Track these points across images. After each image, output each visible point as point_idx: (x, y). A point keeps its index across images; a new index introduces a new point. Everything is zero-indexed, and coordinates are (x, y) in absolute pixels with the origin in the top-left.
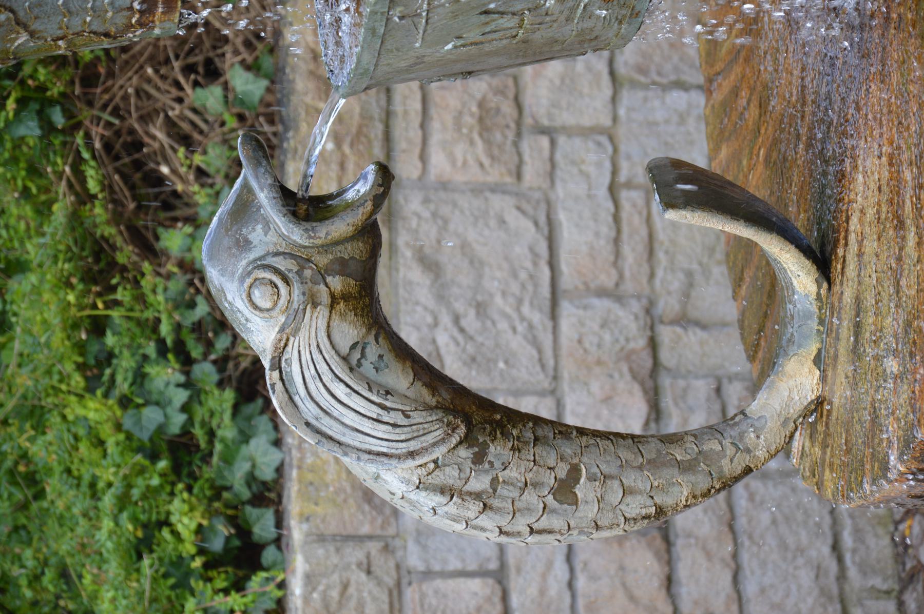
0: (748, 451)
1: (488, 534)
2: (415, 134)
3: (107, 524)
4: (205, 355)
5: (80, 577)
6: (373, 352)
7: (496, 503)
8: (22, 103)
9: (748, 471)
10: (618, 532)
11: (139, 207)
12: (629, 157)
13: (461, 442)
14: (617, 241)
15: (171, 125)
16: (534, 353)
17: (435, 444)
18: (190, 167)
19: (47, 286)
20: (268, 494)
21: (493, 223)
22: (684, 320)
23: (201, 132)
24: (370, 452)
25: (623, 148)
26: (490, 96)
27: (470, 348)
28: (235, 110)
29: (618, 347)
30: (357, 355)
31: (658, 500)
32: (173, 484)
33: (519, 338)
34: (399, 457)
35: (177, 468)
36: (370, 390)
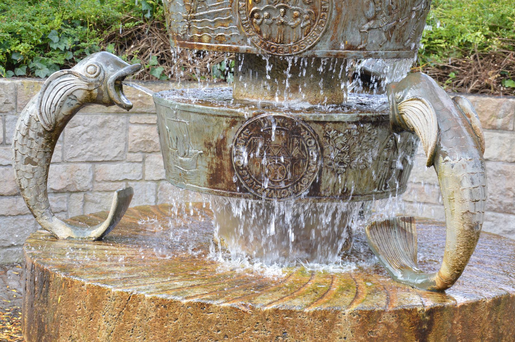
0: (42, 217)
1: (15, 137)
2: (143, 121)
3: (21, 24)
4: (75, 56)
5: (4, 15)
6: (74, 102)
7: (25, 139)
8: (152, 5)
9: (35, 217)
10: (16, 177)
11: (121, 38)
12: (135, 185)
13: (45, 129)
14: (110, 181)
15: (146, 49)
16: (75, 156)
17: (44, 121)
18: (133, 54)
19: (96, 9)
20: (30, 73)
21: (116, 144)
22: (85, 201)
23: (144, 58)
24: (41, 101)
25: (138, 183)
26: (154, 144)
27: (77, 136)
28: (150, 68)
29: (77, 181)
30: (73, 97)
31: (26, 189)
32: (34, 44)
33: (80, 151)
34: (40, 109)
35: (39, 46)
36: (62, 101)
